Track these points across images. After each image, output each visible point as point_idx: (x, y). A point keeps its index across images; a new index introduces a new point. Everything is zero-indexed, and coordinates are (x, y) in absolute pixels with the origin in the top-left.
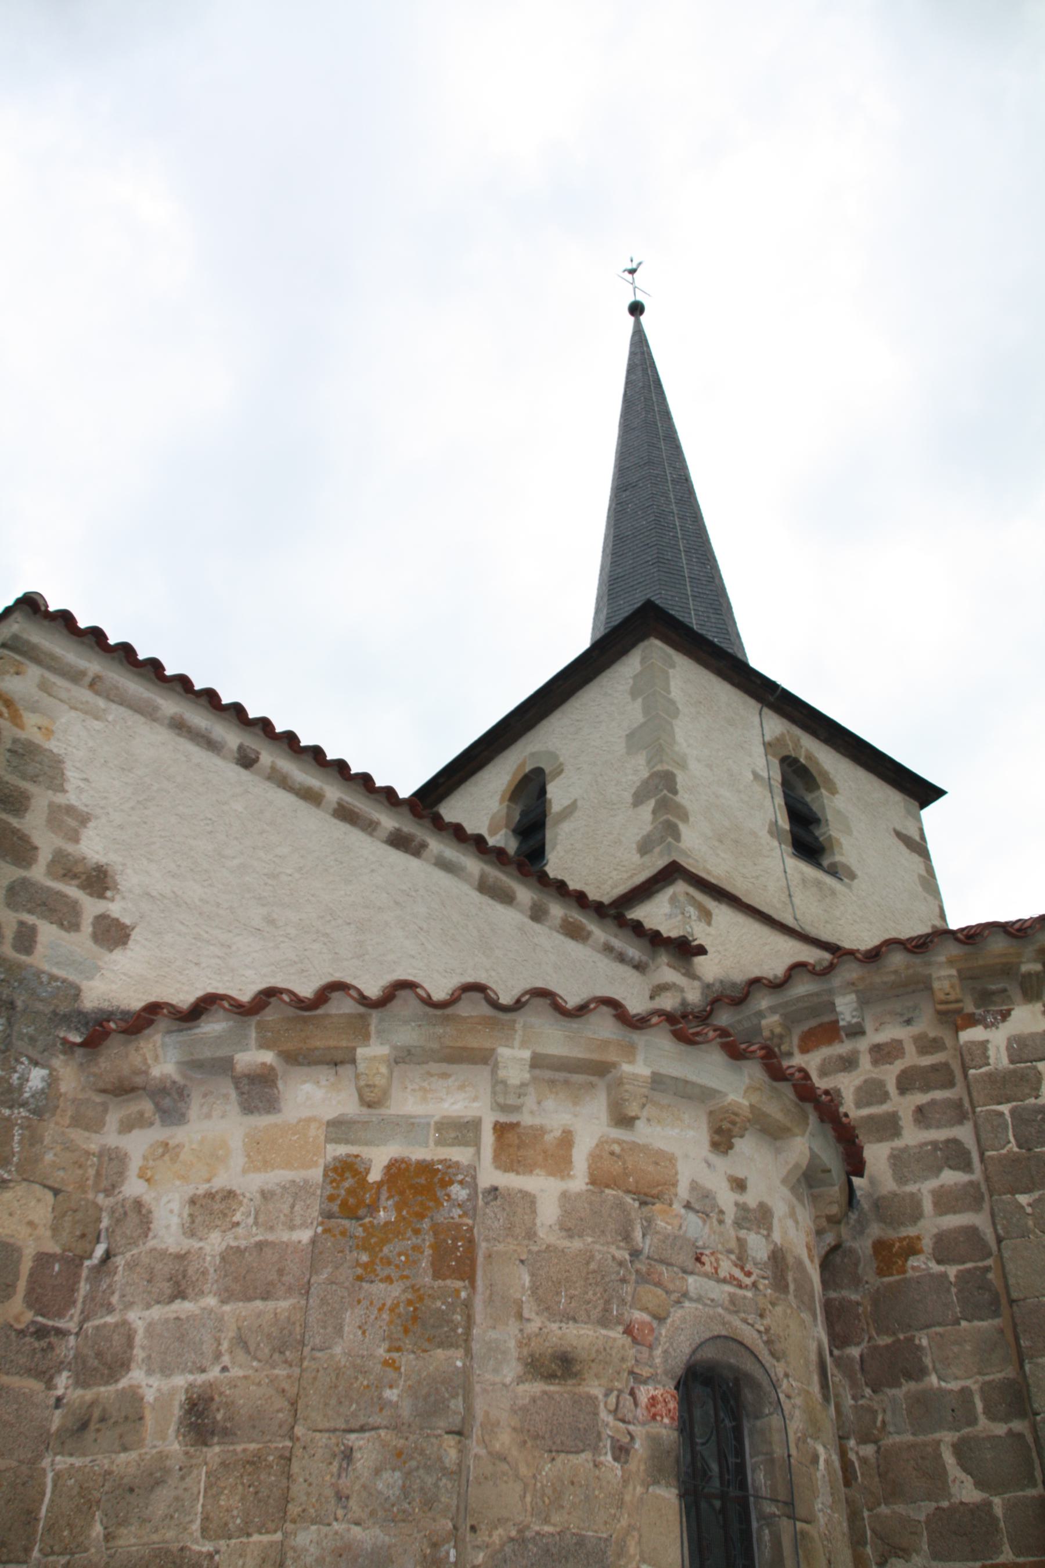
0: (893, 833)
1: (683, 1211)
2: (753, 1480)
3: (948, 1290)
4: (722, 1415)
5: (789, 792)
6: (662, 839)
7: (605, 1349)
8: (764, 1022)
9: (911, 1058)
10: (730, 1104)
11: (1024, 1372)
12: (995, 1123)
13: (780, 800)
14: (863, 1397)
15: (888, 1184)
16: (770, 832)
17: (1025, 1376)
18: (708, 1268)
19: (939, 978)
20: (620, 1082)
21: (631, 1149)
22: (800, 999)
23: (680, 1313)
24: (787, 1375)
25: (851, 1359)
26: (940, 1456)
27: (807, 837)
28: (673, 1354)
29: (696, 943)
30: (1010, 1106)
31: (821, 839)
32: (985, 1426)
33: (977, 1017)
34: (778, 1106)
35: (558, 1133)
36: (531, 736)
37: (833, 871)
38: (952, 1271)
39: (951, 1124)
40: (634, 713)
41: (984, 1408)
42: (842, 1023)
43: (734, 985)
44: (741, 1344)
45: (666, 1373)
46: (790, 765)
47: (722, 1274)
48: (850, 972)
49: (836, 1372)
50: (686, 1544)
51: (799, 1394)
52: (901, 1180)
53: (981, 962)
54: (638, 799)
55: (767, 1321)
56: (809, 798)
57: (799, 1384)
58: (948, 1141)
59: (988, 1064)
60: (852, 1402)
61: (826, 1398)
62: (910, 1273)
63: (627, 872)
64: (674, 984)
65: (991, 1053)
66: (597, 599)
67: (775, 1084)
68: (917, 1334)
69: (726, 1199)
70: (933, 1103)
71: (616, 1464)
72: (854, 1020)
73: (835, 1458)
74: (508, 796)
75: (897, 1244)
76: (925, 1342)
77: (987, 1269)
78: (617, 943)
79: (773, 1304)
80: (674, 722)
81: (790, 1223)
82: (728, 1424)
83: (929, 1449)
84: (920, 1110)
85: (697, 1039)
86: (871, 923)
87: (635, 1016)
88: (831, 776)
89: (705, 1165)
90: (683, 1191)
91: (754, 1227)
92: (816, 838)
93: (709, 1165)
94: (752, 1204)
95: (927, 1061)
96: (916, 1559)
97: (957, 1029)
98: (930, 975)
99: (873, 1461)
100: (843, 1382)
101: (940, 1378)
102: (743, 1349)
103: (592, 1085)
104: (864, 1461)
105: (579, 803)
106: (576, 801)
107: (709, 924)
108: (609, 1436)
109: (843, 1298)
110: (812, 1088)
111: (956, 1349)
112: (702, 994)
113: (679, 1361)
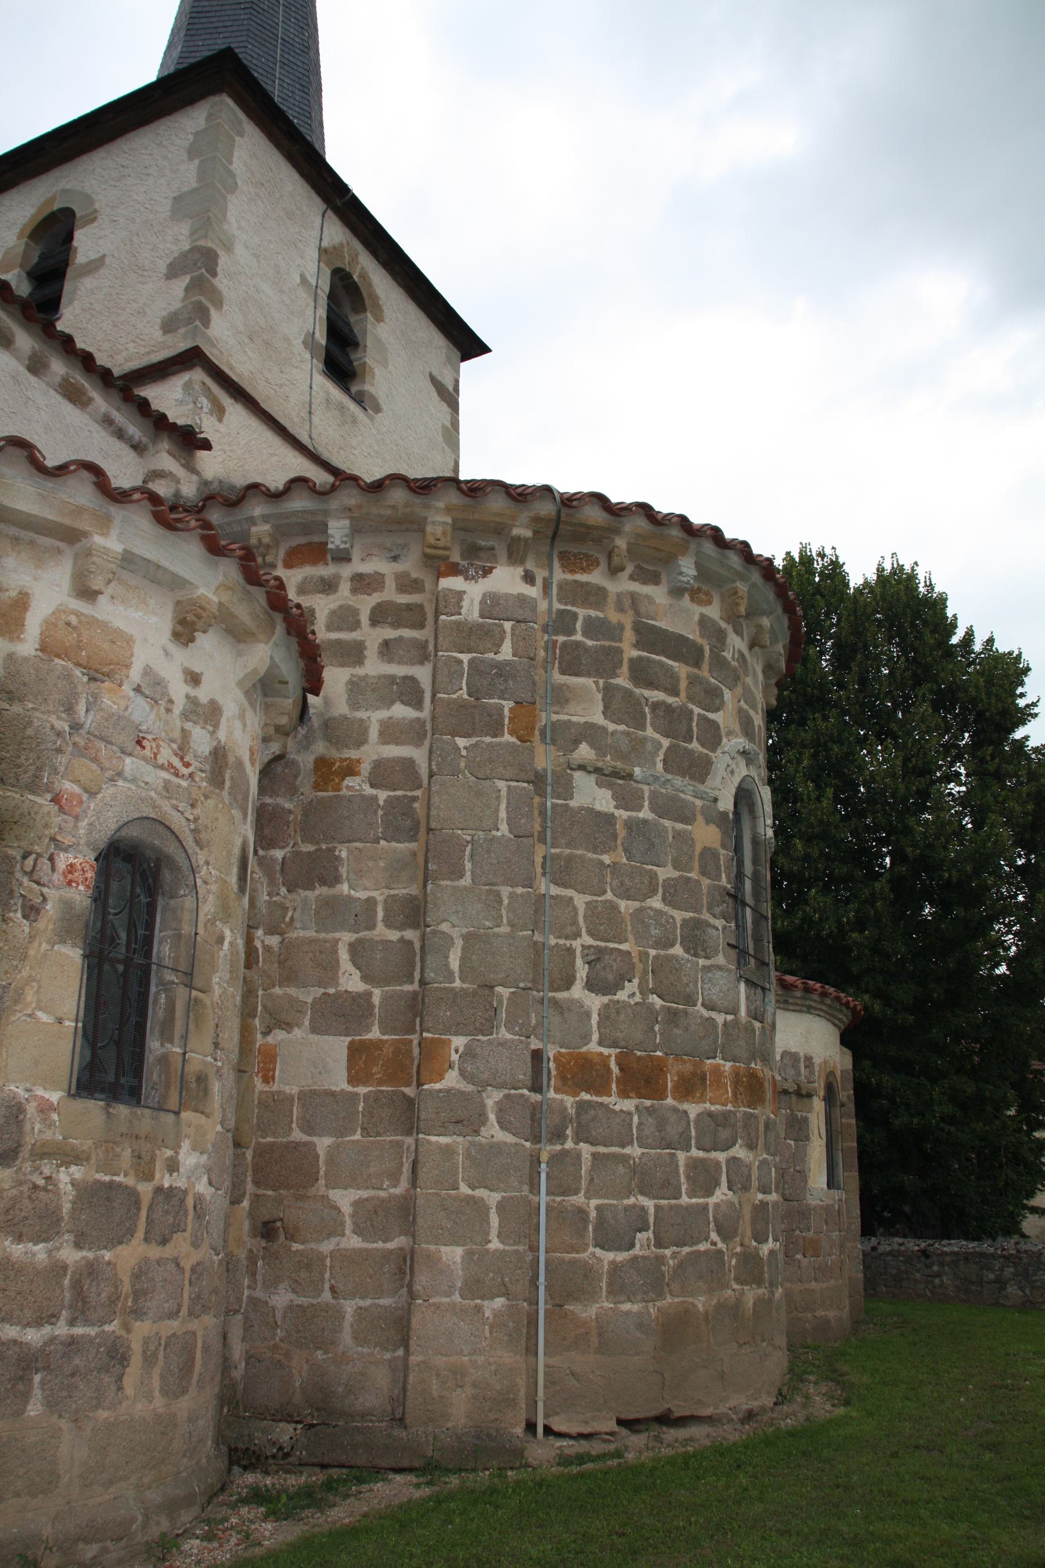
0: (428, 376)
1: (132, 694)
2: (159, 952)
3: (376, 812)
4: (138, 890)
5: (333, 307)
6: (190, 321)
7: (29, 813)
8: (254, 529)
9: (389, 594)
10: (198, 597)
11: (426, 891)
12: (453, 669)
13: (322, 312)
14: (278, 894)
15: (341, 708)
16: (305, 343)
17: (425, 894)
18: (147, 752)
19: (433, 523)
20: (88, 553)
21: (88, 623)
22: (295, 513)
23: (111, 791)
24: (207, 863)
25: (273, 860)
26: (336, 952)
27: (341, 358)
28: (98, 827)
29: (202, 436)
30: (470, 656)
31: (355, 364)
32: (382, 932)
33: (460, 568)
34: (248, 608)
35: (13, 594)
36: (66, 169)
37: (360, 399)
38: (383, 795)
39: (412, 662)
40: (188, 174)
41: (384, 916)
42: (330, 546)
43: (232, 487)
44: (169, 828)
45: (88, 844)
46: (341, 279)
47: (161, 760)
48: (350, 497)
49: (257, 869)
50: (83, 998)
51: (216, 882)
52: (354, 705)
53: (477, 516)
54: (173, 272)
55: (197, 811)
56: (353, 319)
57: (218, 873)
58: (406, 677)
59: (460, 614)
60: (267, 898)
61: (242, 889)
62: (344, 792)
63: (145, 346)
64: (171, 473)
65: (465, 604)
66: (173, 30)
67: (249, 587)
68: (339, 846)
69: (178, 690)
70: (400, 639)
71: (25, 921)
72: (343, 546)
73: (240, 943)
74: (28, 232)
75: (338, 764)
76: (344, 854)
77: (415, 799)
78: (118, 417)
79: (206, 797)
80: (229, 197)
81: (238, 724)
82: (144, 899)
83: (328, 945)
84: (386, 644)
85: (179, 525)
86: (384, 460)
87: (116, 489)
88: (381, 303)
89: (163, 653)
90: (135, 674)
91: (201, 722)
92: (351, 362)
93: (167, 654)
94: (204, 699)
95: (403, 599)
96: (297, 1032)
97: (440, 575)
98: (426, 518)
99: (276, 949)
100: (262, 879)
101: (350, 887)
102: (168, 833)
103: (59, 551)
104: (268, 949)
105: (108, 260)
106: (104, 256)
107: (220, 420)
108: (22, 895)
109: (277, 805)
110: (285, 599)
111: (370, 864)
112: (198, 489)
113: (103, 836)
